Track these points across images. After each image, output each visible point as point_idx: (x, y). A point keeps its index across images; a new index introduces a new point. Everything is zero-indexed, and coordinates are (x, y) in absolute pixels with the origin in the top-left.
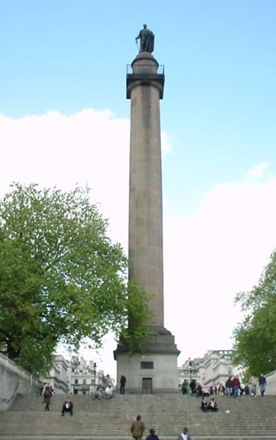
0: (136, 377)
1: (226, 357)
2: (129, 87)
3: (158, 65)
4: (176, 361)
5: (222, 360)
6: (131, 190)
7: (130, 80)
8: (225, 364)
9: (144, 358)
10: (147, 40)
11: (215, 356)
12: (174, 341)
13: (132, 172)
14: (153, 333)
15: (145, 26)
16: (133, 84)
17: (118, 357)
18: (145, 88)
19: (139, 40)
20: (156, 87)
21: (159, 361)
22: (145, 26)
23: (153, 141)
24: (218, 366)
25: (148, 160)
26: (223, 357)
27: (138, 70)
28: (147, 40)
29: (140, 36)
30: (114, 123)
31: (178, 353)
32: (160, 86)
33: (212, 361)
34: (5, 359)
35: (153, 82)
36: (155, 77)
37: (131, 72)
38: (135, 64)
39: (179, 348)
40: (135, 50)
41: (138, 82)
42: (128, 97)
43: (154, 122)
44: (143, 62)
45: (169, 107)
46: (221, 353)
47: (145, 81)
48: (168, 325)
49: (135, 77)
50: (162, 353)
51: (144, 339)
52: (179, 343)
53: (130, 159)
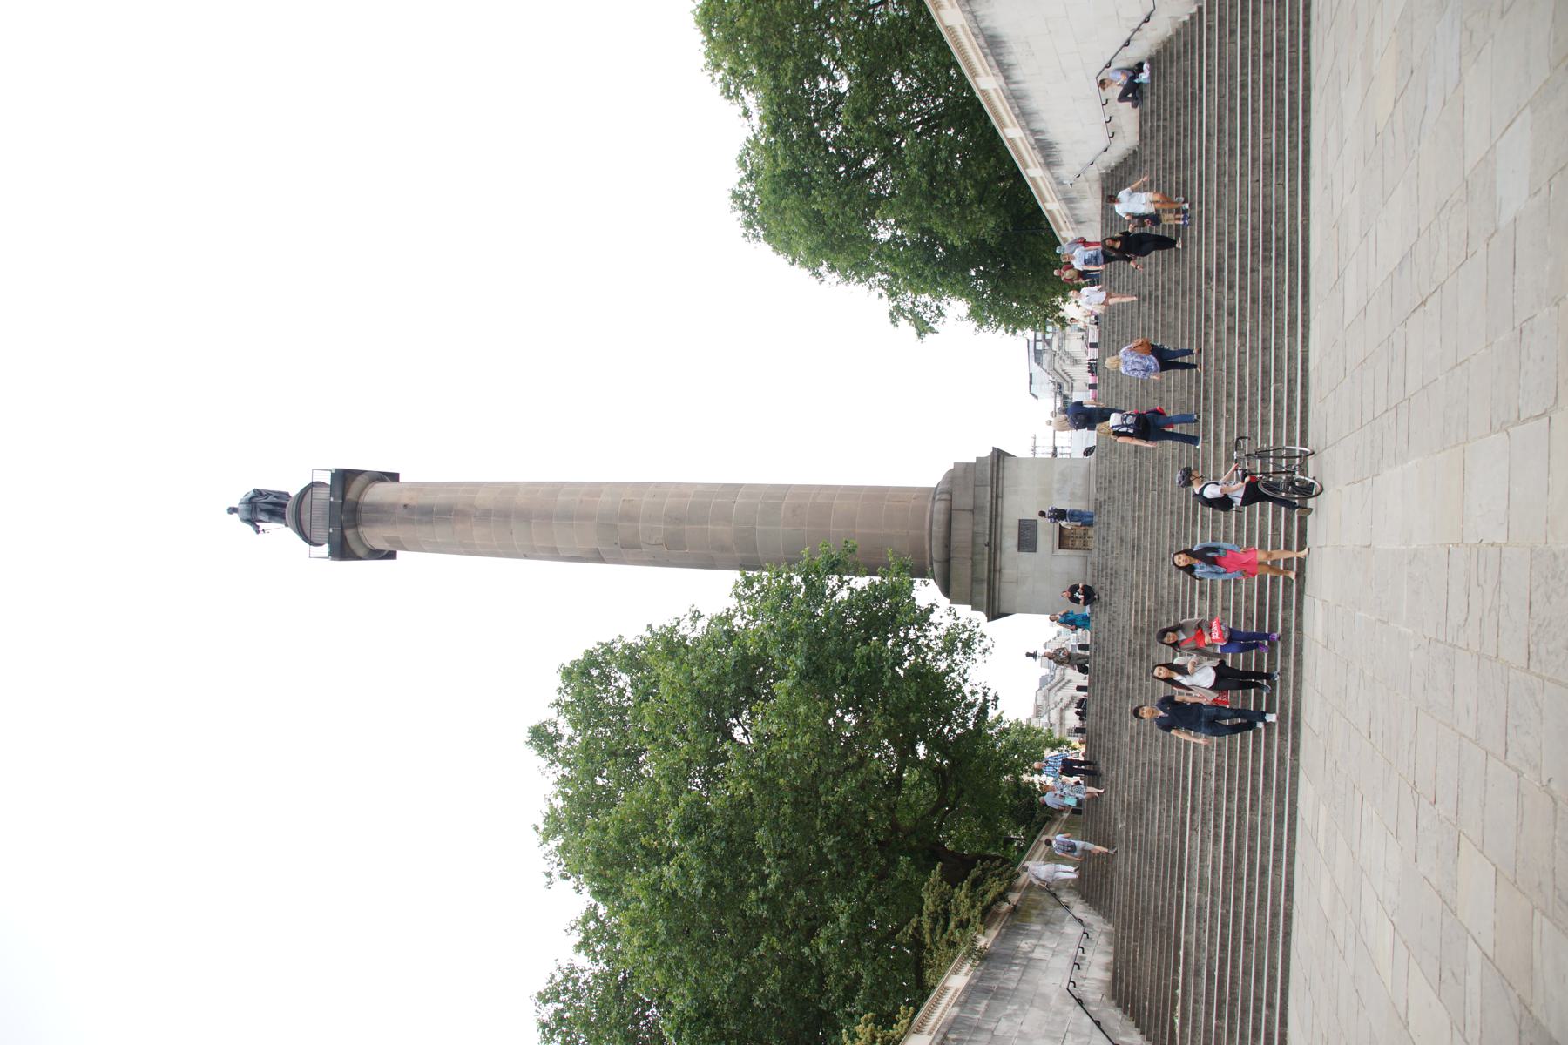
0: (1053, 567)
1: (1048, 336)
2: (361, 552)
3: (313, 485)
4: (1019, 460)
5: (1055, 346)
6: (597, 557)
7: (342, 551)
8: (1063, 338)
9: (1010, 540)
10: (263, 507)
11: (1046, 358)
12: (968, 464)
13: (554, 554)
14: (1120, 440)
15: (232, 510)
16: (354, 546)
17: (1003, 610)
18: (363, 516)
19: (262, 526)
20: (362, 491)
21: (1021, 504)
22: (232, 510)
23: (482, 500)
24: (1067, 353)
25: (525, 516)
26: (1048, 342)
27: (321, 532)
28: (263, 507)
29: (252, 521)
30: (418, 582)
31: (999, 456)
32: (360, 480)
33: (1057, 367)
34: (946, 989)
35: (351, 496)
36: (338, 493)
37: (325, 549)
38: (307, 532)
39: (986, 452)
40: (280, 534)
41: (349, 534)
42: (391, 555)
43: (440, 499)
44: (305, 517)
45: (423, 460)
46: (1040, 346)
47: (347, 515)
48: (928, 473)
49: (338, 539)
50: (997, 497)
51: (965, 533)
52: (975, 450)
53: (526, 557)
